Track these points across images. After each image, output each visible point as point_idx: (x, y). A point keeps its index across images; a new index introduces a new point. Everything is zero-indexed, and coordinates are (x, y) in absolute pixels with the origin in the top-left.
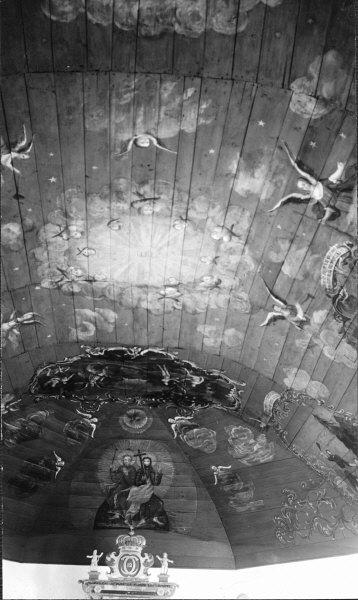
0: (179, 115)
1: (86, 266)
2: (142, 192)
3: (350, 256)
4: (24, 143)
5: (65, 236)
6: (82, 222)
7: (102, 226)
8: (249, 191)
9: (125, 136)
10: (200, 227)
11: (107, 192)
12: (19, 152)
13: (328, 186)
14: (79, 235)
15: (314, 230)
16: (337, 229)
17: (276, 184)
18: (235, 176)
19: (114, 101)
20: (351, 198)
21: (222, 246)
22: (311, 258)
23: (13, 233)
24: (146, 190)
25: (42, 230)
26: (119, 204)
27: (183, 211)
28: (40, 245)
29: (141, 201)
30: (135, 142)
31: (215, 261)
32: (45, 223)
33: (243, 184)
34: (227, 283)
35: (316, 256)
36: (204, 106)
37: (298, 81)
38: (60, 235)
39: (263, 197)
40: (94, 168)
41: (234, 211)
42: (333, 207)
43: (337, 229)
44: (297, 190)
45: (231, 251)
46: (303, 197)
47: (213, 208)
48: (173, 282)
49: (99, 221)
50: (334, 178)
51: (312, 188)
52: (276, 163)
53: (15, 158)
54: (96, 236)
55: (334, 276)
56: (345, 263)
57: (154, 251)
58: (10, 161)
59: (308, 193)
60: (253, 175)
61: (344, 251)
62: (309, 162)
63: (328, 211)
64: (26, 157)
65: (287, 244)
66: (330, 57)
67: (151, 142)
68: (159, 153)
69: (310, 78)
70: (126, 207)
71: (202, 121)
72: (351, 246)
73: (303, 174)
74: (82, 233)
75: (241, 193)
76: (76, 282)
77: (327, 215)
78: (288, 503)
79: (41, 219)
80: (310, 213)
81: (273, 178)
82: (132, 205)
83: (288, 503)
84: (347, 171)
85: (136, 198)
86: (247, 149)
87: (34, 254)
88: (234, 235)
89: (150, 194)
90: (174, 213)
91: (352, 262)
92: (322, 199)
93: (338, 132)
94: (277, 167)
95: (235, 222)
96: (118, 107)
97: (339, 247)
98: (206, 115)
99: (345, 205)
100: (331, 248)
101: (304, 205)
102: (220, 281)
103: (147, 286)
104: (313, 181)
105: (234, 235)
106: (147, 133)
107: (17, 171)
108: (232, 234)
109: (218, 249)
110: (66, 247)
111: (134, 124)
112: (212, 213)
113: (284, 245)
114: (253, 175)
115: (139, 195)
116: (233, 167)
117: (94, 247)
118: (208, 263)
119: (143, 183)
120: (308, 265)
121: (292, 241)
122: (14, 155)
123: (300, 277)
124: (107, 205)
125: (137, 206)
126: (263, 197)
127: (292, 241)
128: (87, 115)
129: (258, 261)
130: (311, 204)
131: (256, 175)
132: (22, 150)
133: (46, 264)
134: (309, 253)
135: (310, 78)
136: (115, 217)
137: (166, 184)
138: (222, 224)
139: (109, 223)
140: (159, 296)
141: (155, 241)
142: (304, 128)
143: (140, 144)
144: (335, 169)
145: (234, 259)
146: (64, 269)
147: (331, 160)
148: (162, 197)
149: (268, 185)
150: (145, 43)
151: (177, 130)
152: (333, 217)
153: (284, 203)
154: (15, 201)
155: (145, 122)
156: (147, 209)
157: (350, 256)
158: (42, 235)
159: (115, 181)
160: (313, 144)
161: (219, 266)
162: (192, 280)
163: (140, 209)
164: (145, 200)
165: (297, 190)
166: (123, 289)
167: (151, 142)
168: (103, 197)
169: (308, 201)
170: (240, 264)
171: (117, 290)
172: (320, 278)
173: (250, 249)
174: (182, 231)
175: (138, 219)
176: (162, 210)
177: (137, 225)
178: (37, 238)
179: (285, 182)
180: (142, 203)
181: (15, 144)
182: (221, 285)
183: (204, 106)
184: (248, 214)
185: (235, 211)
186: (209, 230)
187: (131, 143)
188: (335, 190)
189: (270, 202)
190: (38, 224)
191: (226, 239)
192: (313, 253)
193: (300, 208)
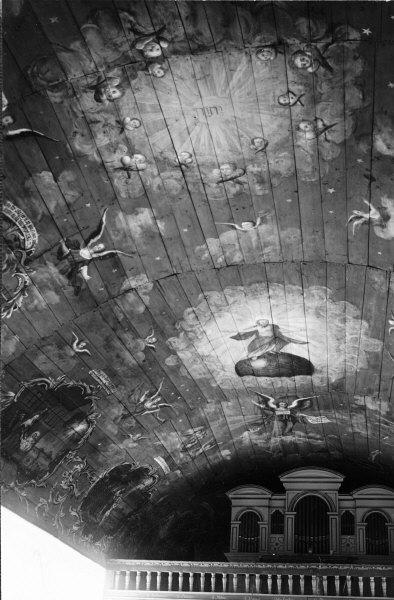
1: (290, 73)
2: (238, 187)
3: (19, 247)
4: (356, 223)
5: (320, 125)
6: (299, 143)
7: (274, 141)
8: (137, 214)
9: (263, 228)
10: (161, 163)
11: (275, 181)
12: (361, 217)
13: (84, 262)
14: (302, 126)
15: (61, 230)
16: (49, 250)
17: (118, 231)
18: (155, 218)
19: (278, 248)
20: (63, 274)
21: (125, 149)
22: (41, 210)
23: (384, 141)
24: (233, 189)
25: (349, 133)
26: (259, 169)
27: (188, 174)
28: (354, 112)
29: (236, 177)
30: (254, 224)
31: (122, 126)
32: (344, 143)
33: (145, 216)
34: (88, 101)
35: (39, 217)
36: (206, 255)
37: (150, 288)
38: (326, 128)
39: (121, 215)
40: (290, 200)
41: (137, 190)
42: (66, 257)
43: (49, 250)
44: (99, 242)
45: (113, 148)
46: (92, 241)
47: (159, 186)
48: (157, 69)
49: (280, 147)
50: (84, 270)
51: (91, 251)
52: (130, 243)
53: (366, 213)
54: (280, 126)
55: (10, 221)
56: (17, 239)
57: (202, 118)
58: (371, 212)
59: (92, 247)
60: (141, 227)
61: (28, 244)
62: (108, 262)
63: (66, 250)
64: (356, 212)
65: (69, 198)
66: (142, 309)
67: (241, 226)
68: (232, 219)
69: (145, 294)
70: (250, 168)
72: (28, 254)
73: (105, 253)
74: (298, 129)
75: (142, 209)
76: (303, 40)
77: (65, 248)
79: (348, 149)
80: (78, 237)
82: (245, 172)
84: (82, 280)
85: (241, 179)
86: (158, 240)
87: (364, 99)
88: (121, 169)
89: (228, 185)
90: (196, 169)
91: (14, 245)
92: (78, 253)
93: (106, 287)
94: (126, 241)
95: (130, 181)
96: (274, 244)
97: (34, 242)
99: (62, 266)
100: (37, 235)
101: (86, 237)
102: (98, 99)
103: (193, 52)
104: (95, 256)
105: (121, 169)
106: (246, 232)
107: (366, 202)
108: (126, 168)
109: (127, 141)
110: (319, 107)
111: (258, 235)
112: (158, 181)
113: (71, 195)
114: (141, 227)
115: (239, 183)
116: (161, 225)
117: (281, 110)
118: (128, 119)
119: (239, 195)
120: (36, 203)
121: (68, 205)
122: (367, 216)
123: (29, 183)
124: (272, 167)
125: (239, 171)
126: (121, 215)
127: (68, 205)
128: (299, 238)
129: (79, 157)
130: (82, 243)
131: (139, 228)
133: (349, 78)
134: (46, 212)
137: (215, 197)
138: (140, 173)
139: (266, 145)
140: (166, 34)
141: (205, 133)
142: (128, 272)
143: (250, 224)
144: (89, 274)
145: (102, 140)
146: (322, 69)
147: (96, 274)
148: (215, 185)
149: (124, 225)
150: (262, 279)
152: (61, 252)
153: (101, 223)
154: (374, 175)
155: (250, 238)
156: (227, 170)
157: (19, 247)
158: (350, 123)
159: (267, 192)
160: (114, 271)
161: (112, 121)
162: (133, 82)
163: (235, 168)
164: (232, 179)
165: (159, 395)
166: (228, 37)
167: (241, 226)
168: (278, 174)
169: (86, 243)
170: (92, 136)
171: (238, 30)
172: (16, 203)
173: (95, 162)
175: (234, 158)
176: (211, 171)
177: (233, 150)
178: (356, 124)
179: (113, 237)
180: (233, 175)
181: (365, 223)
182: (91, 94)
183: (206, 255)
184: (123, 195)
185: (137, 191)
186: (150, 163)
187: (258, 223)
188: (77, 264)
189: (112, 217)
190: (353, 143)
191: (127, 159)
192: (43, 215)
193: (87, 234)
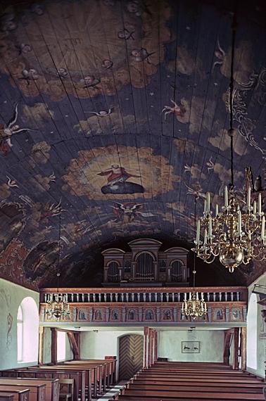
0: (90, 126)
2: (96, 90)
13: (7, 136)
14: (133, 53)
23: (183, 64)
30: (108, 113)
46: (11, 124)
50: (9, 140)
54: (120, 52)
59: (11, 127)
71: (78, 125)
78: (209, 167)
81: (30, 119)
82: (100, 81)
83: (209, 167)
88: (23, 78)
95: (30, 86)
98: (78, 128)
106: (102, 117)
108: (27, 78)
115: (97, 88)
130: (5, 125)
132: (169, 110)
135: (46, 152)
136: (109, 70)
151: (88, 120)
169: (8, 126)
174: (58, 68)
179: (24, 121)
